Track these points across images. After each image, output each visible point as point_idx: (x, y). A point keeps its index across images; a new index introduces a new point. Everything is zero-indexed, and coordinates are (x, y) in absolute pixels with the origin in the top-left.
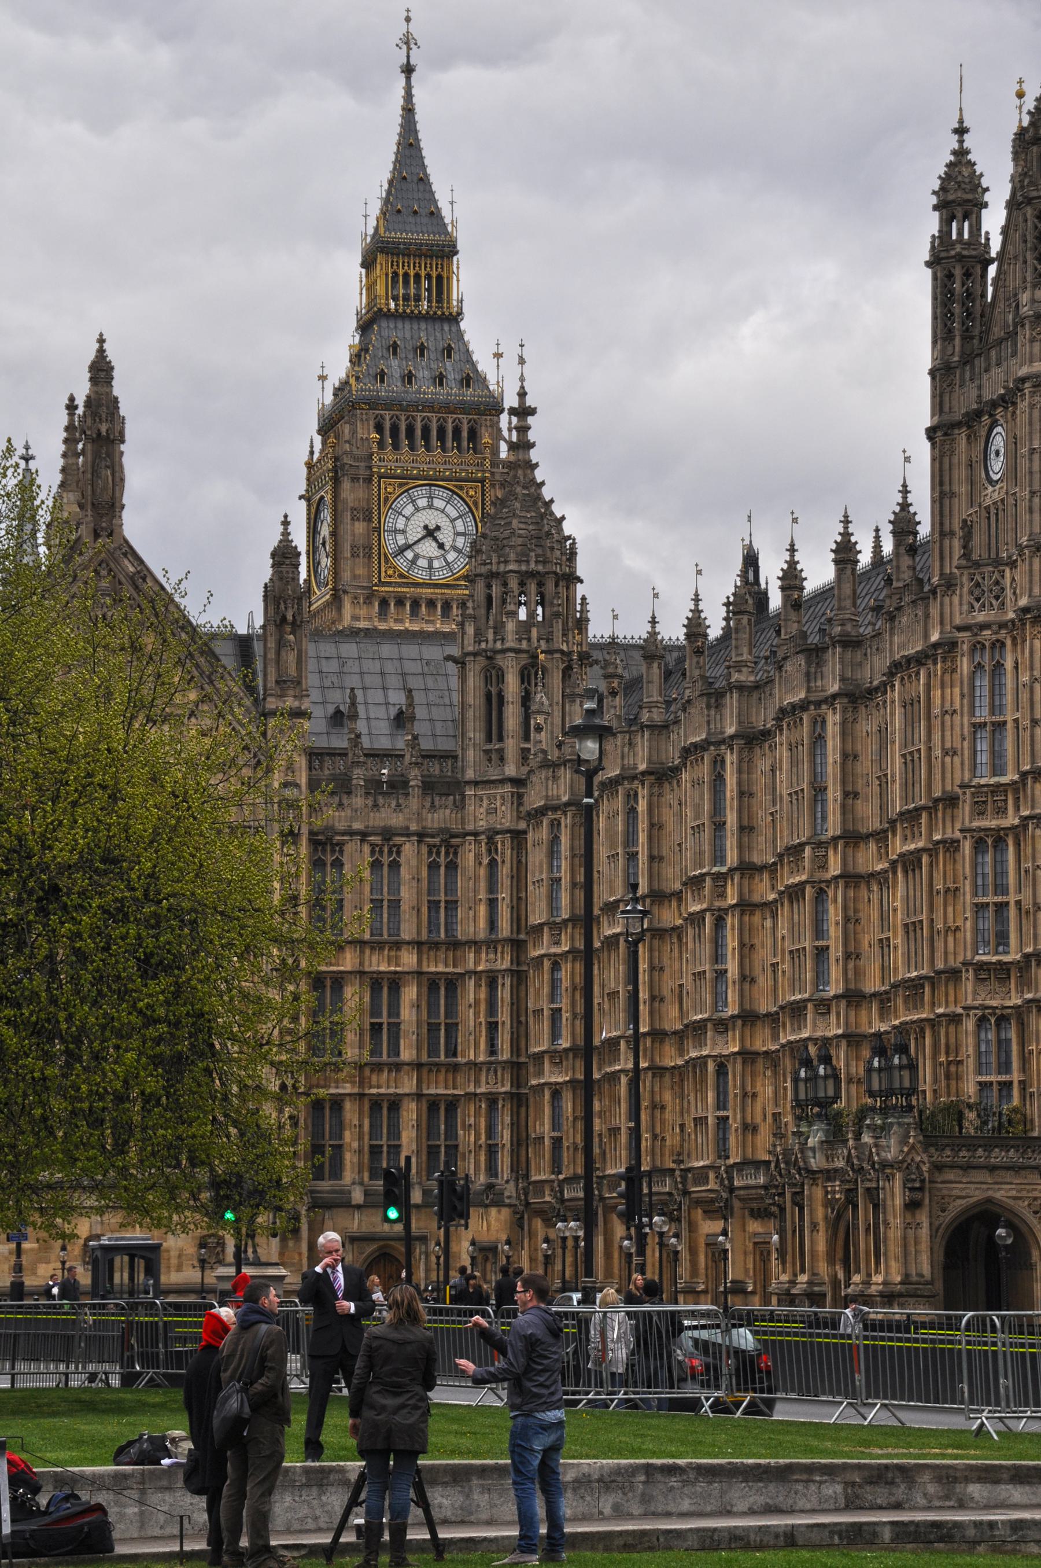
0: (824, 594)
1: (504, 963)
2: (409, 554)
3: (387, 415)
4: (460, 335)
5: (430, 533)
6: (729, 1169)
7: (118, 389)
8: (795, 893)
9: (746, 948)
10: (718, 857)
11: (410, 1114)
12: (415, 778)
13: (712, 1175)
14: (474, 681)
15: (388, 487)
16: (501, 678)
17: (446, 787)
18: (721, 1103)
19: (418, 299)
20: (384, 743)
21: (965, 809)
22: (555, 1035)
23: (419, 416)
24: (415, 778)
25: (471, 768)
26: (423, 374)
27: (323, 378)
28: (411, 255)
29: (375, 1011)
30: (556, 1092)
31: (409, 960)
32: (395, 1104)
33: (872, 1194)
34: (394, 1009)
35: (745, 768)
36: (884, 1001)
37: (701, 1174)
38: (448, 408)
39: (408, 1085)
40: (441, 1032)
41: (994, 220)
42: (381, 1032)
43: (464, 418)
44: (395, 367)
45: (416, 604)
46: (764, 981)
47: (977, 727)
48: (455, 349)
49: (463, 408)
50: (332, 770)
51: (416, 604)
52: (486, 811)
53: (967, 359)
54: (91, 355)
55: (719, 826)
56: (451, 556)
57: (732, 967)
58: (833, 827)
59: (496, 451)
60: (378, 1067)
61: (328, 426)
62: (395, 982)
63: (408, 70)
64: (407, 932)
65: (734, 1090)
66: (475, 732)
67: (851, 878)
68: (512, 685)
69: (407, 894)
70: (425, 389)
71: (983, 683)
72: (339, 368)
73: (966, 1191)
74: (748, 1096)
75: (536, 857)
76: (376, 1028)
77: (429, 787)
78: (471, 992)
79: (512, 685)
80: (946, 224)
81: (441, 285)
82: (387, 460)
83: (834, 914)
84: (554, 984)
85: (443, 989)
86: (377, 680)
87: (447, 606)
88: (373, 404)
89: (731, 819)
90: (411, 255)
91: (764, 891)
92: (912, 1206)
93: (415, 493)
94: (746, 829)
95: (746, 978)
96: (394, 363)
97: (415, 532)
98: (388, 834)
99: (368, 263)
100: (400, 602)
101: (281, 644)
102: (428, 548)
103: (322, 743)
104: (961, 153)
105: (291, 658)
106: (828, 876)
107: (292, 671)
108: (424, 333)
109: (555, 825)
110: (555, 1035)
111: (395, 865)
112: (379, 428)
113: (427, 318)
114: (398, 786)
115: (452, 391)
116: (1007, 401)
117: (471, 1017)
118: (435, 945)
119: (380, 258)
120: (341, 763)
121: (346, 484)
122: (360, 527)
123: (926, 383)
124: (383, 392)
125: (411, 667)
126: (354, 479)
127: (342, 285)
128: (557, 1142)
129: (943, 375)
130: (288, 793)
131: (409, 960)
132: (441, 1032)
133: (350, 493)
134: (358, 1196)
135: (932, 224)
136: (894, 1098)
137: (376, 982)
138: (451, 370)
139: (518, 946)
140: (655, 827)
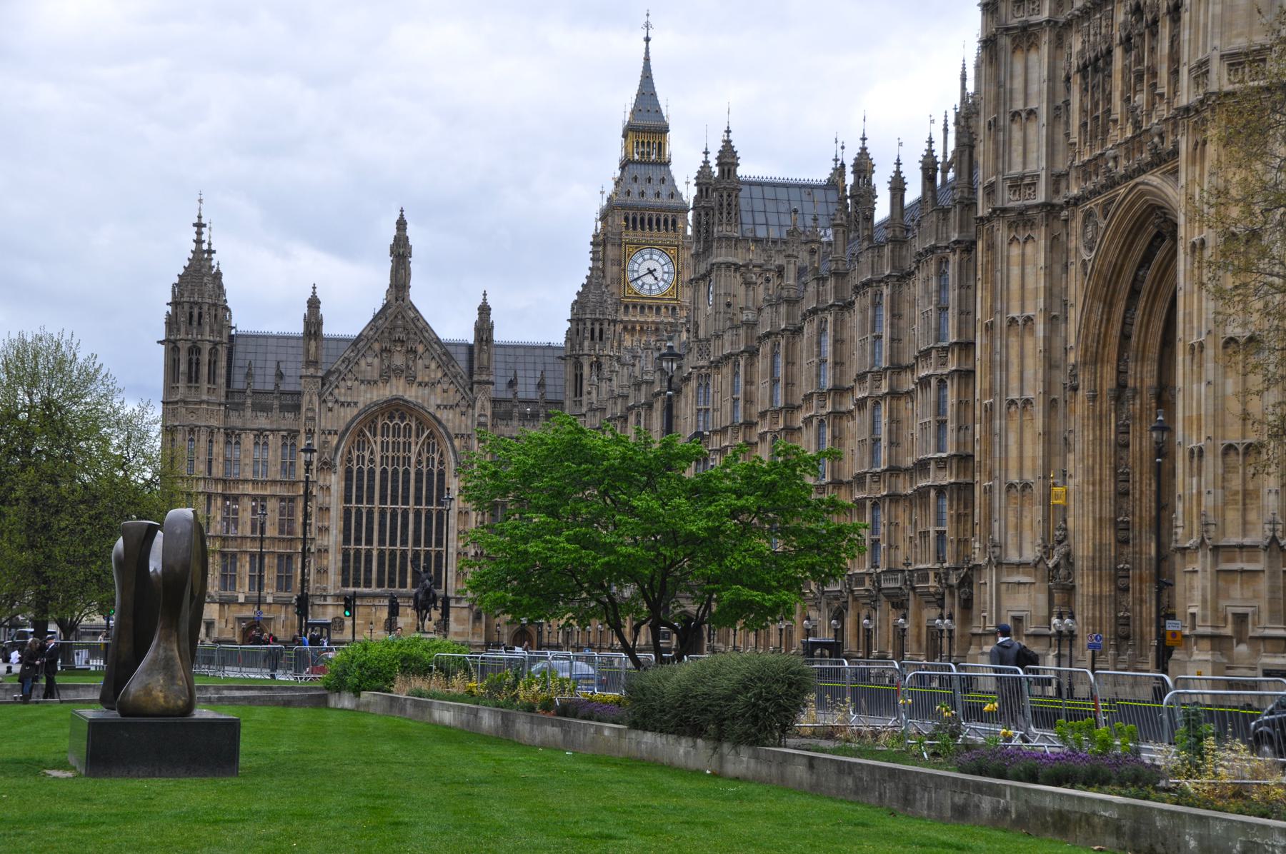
2: (640, 282)
3: (631, 213)
4: (669, 172)
5: (651, 272)
13: (867, 579)
15: (630, 249)
16: (581, 367)
19: (649, 154)
20: (532, 396)
23: (647, 213)
26: (650, 192)
27: (602, 193)
38: (662, 209)
43: (670, 214)
44: (635, 189)
45: (643, 307)
47: (699, 410)
49: (669, 209)
51: (643, 307)
56: (661, 284)
59: (685, 231)
61: (604, 217)
63: (647, 40)
70: (650, 199)
81: (661, 148)
82: (630, 235)
86: (532, 366)
87: (658, 309)
88: (623, 207)
93: (643, 252)
96: (635, 186)
97: (643, 270)
99: (625, 136)
100: (635, 307)
101: (481, 350)
102: (649, 279)
103: (502, 395)
105: (485, 356)
107: (486, 363)
112: (626, 219)
113: (654, 163)
114: (535, 416)
115: (664, 200)
119: (630, 134)
120: (509, 405)
121: (609, 247)
122: (616, 269)
124: (629, 200)
125: (548, 360)
126: (613, 245)
127: (614, 150)
128: (941, 535)
130: (482, 419)
138: (664, 191)
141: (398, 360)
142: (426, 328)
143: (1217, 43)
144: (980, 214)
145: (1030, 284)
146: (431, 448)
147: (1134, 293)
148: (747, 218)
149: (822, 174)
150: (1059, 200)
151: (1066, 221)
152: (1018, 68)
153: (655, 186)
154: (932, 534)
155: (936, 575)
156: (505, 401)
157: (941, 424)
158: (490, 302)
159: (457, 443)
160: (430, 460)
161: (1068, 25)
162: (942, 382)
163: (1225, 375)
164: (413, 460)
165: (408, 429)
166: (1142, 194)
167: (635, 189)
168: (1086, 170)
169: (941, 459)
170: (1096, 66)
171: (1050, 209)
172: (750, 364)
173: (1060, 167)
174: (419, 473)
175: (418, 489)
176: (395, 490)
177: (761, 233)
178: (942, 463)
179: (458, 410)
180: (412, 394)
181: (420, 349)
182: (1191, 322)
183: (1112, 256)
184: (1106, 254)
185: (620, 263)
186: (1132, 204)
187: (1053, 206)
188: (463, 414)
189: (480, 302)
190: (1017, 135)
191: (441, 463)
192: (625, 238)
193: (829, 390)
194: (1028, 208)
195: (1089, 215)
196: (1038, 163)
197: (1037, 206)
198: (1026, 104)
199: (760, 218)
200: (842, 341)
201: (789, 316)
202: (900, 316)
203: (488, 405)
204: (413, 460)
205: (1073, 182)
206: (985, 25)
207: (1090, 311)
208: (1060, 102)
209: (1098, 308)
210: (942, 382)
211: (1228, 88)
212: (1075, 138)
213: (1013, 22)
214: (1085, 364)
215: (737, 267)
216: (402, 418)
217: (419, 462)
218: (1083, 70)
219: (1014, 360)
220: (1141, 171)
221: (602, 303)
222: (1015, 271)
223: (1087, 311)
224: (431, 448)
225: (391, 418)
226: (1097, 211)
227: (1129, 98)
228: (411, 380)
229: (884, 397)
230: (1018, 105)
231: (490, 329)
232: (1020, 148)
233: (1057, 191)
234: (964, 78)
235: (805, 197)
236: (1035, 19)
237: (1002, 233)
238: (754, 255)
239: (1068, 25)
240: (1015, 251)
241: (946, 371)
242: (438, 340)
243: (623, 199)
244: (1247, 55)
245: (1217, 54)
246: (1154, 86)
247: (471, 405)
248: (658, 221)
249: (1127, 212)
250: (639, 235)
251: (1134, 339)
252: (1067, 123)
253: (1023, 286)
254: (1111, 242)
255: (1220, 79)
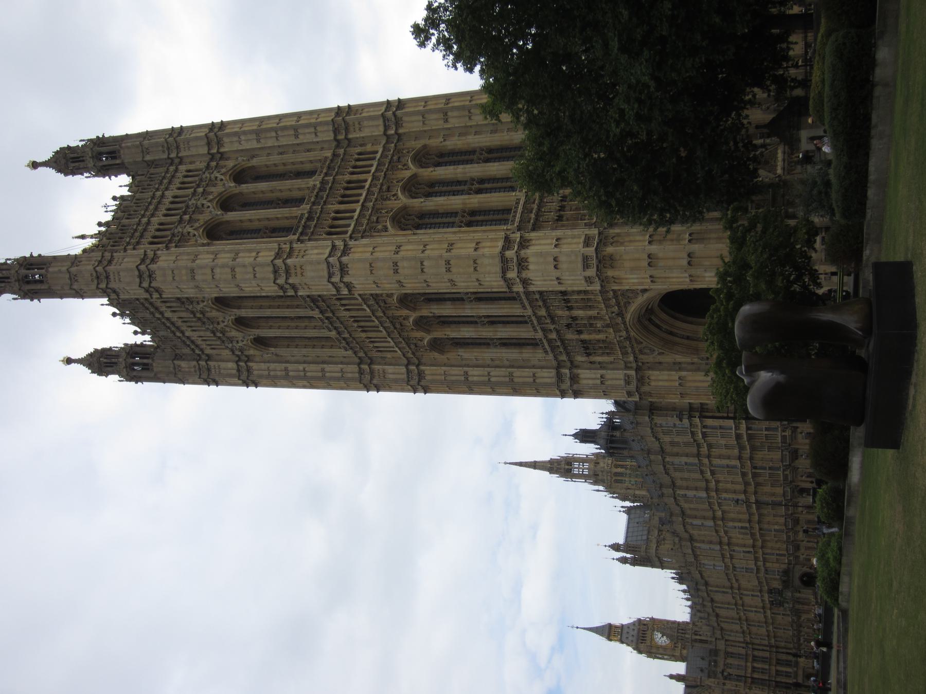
1: (750, 646)
11: (780, 668)
14: (696, 644)
17: (715, 652)
18: (765, 468)
25: (712, 647)
26: (632, 633)
28: (610, 632)
31: (749, 664)
32: (777, 671)
35: (717, 602)
37: (788, 537)
40: (764, 660)
41: (628, 556)
42: (763, 671)
44: (630, 638)
48: (628, 626)
52: (721, 645)
68: (698, 637)
69: (736, 663)
72: (630, 649)
73: (797, 582)
75: (730, 638)
77: (716, 656)
78: (756, 653)
79: (698, 637)
81: (616, 627)
82: (648, 643)
83: (745, 592)
85: (755, 659)
88: (637, 644)
90: (610, 632)
94: (729, 604)
99: (611, 640)
114: (715, 662)
117: (760, 654)
128: (767, 429)
129: (653, 566)
132: (764, 660)
135: (628, 565)
136: (780, 593)
139: (747, 643)
145: (666, 377)
147: (671, 333)
148: (639, 543)
149: (625, 517)
150: (634, 365)
152: (585, 382)
155: (784, 431)
157: (721, 427)
161: (572, 362)
162: (705, 427)
167: (630, 638)
168: (625, 354)
171: (638, 369)
172: (696, 541)
173: (622, 364)
178: (737, 428)
195: (641, 352)
196: (620, 374)
199: (639, 538)
206: (570, 397)
210: (705, 427)
211: (595, 269)
212: (611, 359)
213: (569, 384)
218: (588, 355)
220: (624, 323)
222: (661, 383)
226: (640, 346)
229: (710, 462)
230: (598, 382)
234: (598, 491)
236: (568, 375)
237: (645, 389)
240: (653, 383)
247: (710, 687)
250: (648, 639)
252: (607, 363)
253: (666, 380)
255: (592, 272)
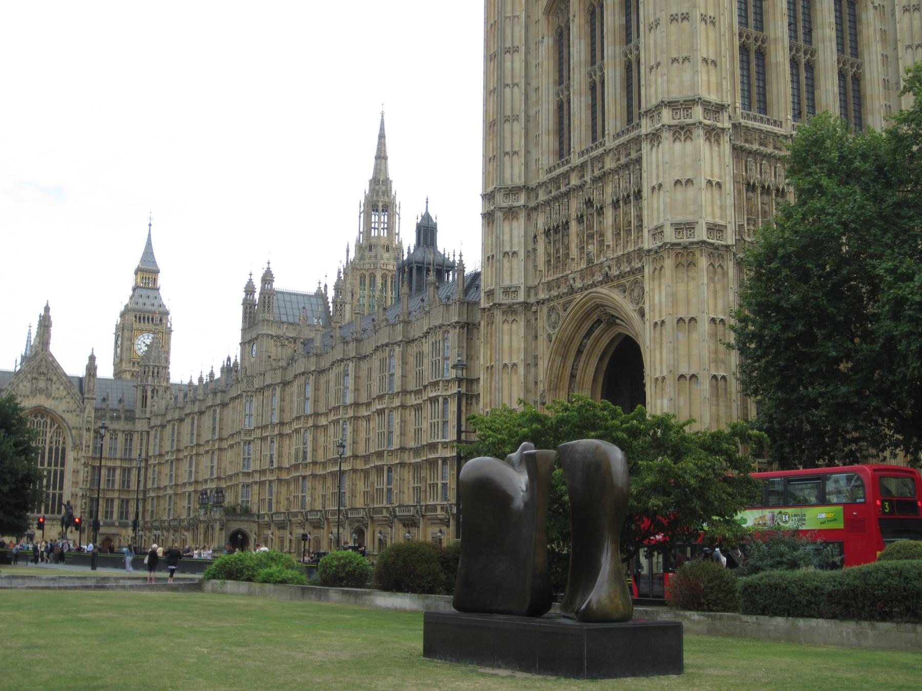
0: (218, 380)
6: (306, 513)
7: (51, 313)
8: (207, 452)
9: (197, 465)
10: (192, 442)
12: (123, 416)
13: (384, 511)
18: (189, 503)
20: (115, 407)
21: (242, 434)
22: (153, 484)
24: (123, 416)
29: (109, 476)
30: (153, 499)
33: (212, 527)
34: (114, 476)
35: (199, 420)
36: (324, 464)
39: (116, 495)
40: (126, 483)
44: (141, 301)
46: (200, 474)
50: (100, 413)
52: (141, 426)
53: (249, 328)
54: (45, 305)
55: (192, 434)
57: (193, 469)
58: (217, 437)
60: (108, 490)
61: (122, 315)
62: (114, 469)
63: (150, 225)
64: (118, 456)
65: (274, 489)
66: (139, 405)
67: (220, 449)
71: (248, 405)
72: (126, 301)
73: (235, 526)
74: (279, 493)
75: (151, 438)
76: (109, 480)
78: (134, 472)
80: (247, 295)
81: (155, 280)
83: (216, 457)
84: (154, 471)
85: (126, 471)
88: (134, 310)
89: (195, 433)
90: (147, 273)
91: (287, 430)
92: (221, 529)
94: (199, 435)
95: (197, 472)
98: (114, 431)
99: (136, 273)
101: (89, 380)
103: (99, 406)
104: (251, 280)
106: (394, 406)
108: (150, 292)
109: (174, 425)
110: (153, 484)
111: (116, 439)
113: (151, 289)
114: (118, 418)
116: (256, 339)
118: (125, 460)
121: (126, 331)
122: (129, 343)
123: (240, 332)
124: (137, 307)
127: (129, 281)
129: (244, 330)
131: (118, 463)
132: (126, 483)
133: (127, 334)
134: (117, 524)
136: (218, 504)
137: (109, 469)
139: (147, 461)
140: (179, 433)
141: (42, 384)
142: (59, 367)
143: (669, 217)
144: (482, 306)
146: (58, 434)
147: (579, 352)
148: (276, 310)
149: (312, 290)
150: (532, 300)
151: (535, 312)
153: (151, 301)
154: (439, 485)
155: (442, 508)
156: (101, 409)
158: (95, 354)
159: (74, 432)
160: (57, 442)
161: (535, 209)
163: (679, 395)
164: (48, 441)
165: (45, 423)
166: (593, 298)
168: (549, 286)
169: (445, 443)
170: (557, 231)
171: (526, 305)
173: (531, 283)
174: (51, 449)
175: (50, 458)
176: (56, 458)
177: (284, 319)
178: (445, 445)
179: (75, 413)
180: (48, 404)
181: (55, 378)
182: (655, 366)
183: (570, 330)
184: (565, 331)
185: (131, 340)
186: (585, 303)
187: (528, 304)
188: (78, 416)
189: (90, 354)
190: (506, 264)
191: (64, 443)
192: (135, 326)
193: (351, 405)
194: (514, 304)
195: (552, 310)
196: (518, 280)
197: (519, 303)
198: (511, 248)
200: (359, 377)
201: (317, 363)
202: (406, 363)
203: (93, 411)
204: (48, 441)
205: (540, 291)
207: (554, 361)
208: (530, 249)
209: (558, 360)
213: (504, 205)
214: (550, 390)
215: (272, 337)
216: (42, 417)
217: (51, 442)
218: (547, 233)
219: (506, 388)
221: (159, 357)
222: (506, 338)
223: (552, 361)
224: (58, 434)
225: (36, 417)
226: (560, 308)
227: (583, 248)
228: (49, 396)
229: (396, 408)
230: (507, 249)
231: (95, 368)
232: (508, 272)
233: (529, 296)
234: (348, 251)
235: (306, 301)
236: (516, 204)
237: (498, 316)
238: (284, 331)
239: (535, 209)
240: (506, 327)
241: (449, 393)
242: (65, 374)
243: (134, 306)
244: (685, 224)
245: (669, 223)
246: (601, 242)
247: (83, 411)
248: (144, 318)
249: (581, 308)
250: (142, 325)
251: (578, 377)
254: (569, 324)
255: (670, 236)
